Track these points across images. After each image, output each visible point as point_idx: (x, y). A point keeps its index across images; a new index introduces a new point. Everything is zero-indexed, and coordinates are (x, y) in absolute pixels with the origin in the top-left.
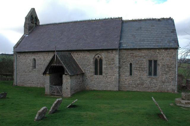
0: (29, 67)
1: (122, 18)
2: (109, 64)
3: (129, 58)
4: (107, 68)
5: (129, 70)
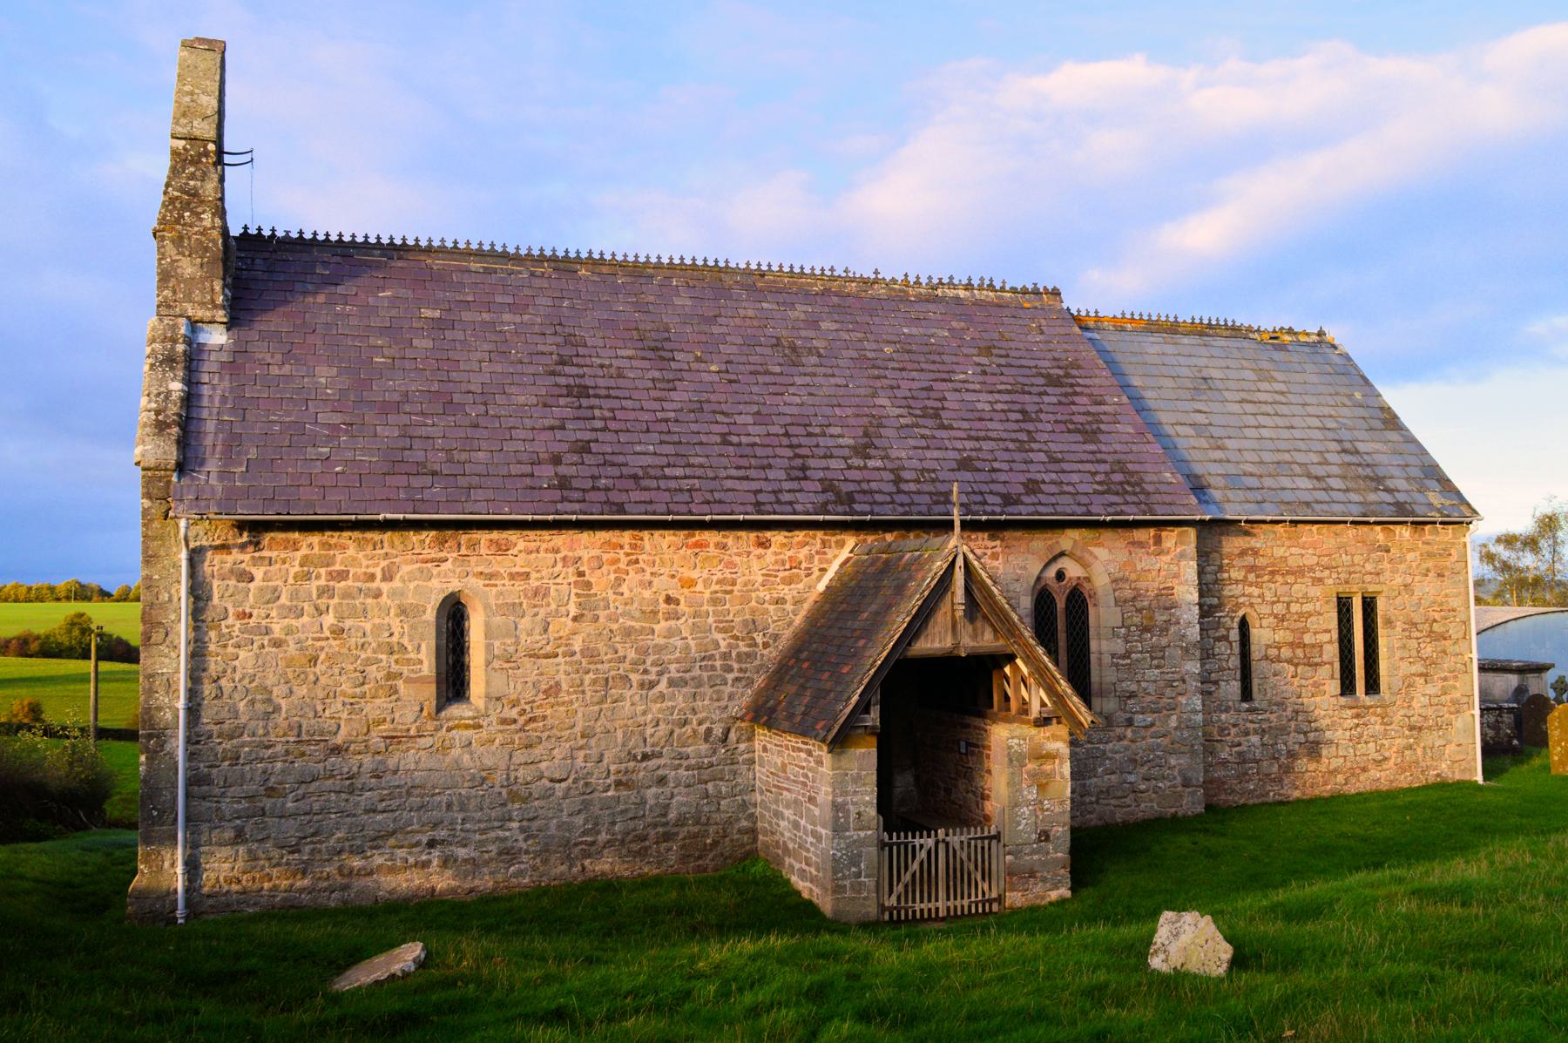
0: (394, 691)
1: (1056, 293)
2: (1146, 629)
3: (1237, 582)
4: (1127, 655)
5: (1235, 662)
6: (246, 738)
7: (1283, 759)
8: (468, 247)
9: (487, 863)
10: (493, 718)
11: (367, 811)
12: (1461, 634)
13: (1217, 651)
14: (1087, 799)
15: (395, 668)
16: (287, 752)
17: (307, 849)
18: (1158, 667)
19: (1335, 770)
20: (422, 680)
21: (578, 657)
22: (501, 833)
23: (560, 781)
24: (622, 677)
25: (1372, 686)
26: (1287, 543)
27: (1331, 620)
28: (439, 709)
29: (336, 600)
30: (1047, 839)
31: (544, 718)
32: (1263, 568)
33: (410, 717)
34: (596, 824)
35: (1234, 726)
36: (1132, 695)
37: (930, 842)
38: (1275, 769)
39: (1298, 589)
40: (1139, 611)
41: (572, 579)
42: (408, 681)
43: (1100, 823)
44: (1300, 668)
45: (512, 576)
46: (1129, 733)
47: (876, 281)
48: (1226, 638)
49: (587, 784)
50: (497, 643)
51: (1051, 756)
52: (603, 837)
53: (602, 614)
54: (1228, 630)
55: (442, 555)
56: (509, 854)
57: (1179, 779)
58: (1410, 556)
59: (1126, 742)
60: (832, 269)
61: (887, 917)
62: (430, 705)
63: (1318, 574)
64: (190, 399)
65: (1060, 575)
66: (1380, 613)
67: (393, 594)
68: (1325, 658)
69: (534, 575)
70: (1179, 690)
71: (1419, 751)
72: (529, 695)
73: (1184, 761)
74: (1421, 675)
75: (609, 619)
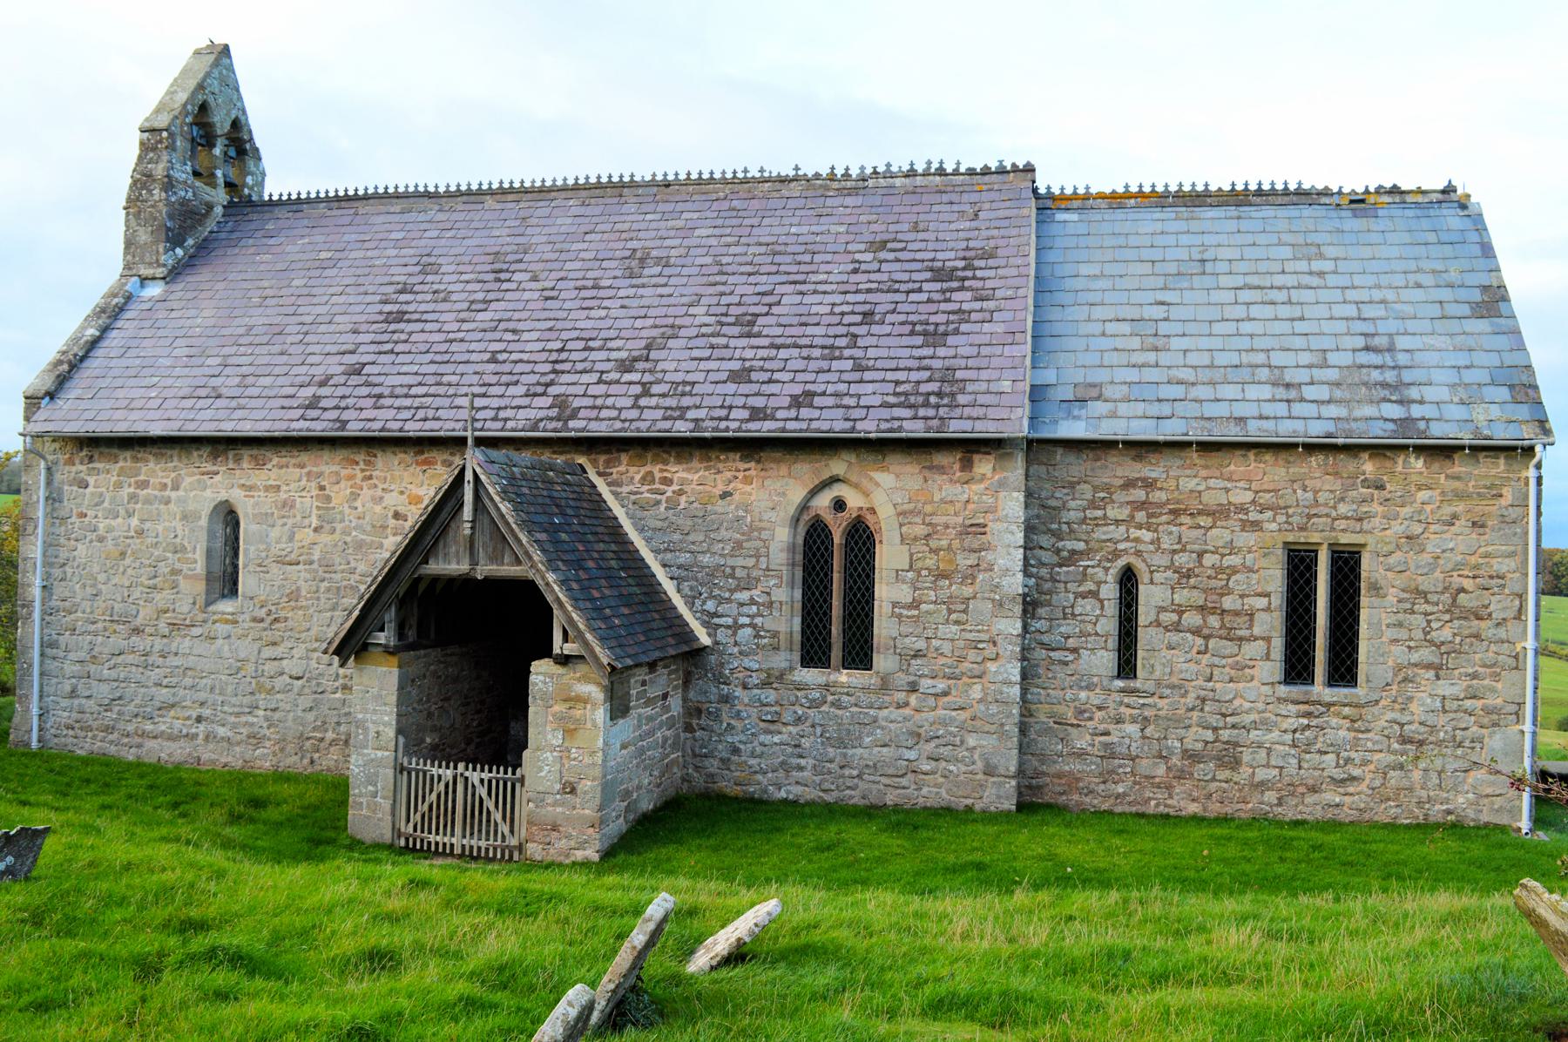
1: (1029, 169)
4: (915, 604)
5: (1109, 625)
6: (79, 614)
7: (1175, 760)
8: (1193, 190)
9: (238, 744)
10: (247, 617)
11: (157, 685)
12: (1510, 614)
13: (1078, 610)
14: (847, 772)
15: (178, 566)
16: (105, 629)
17: (116, 709)
18: (957, 622)
19: (1262, 783)
20: (195, 577)
21: (315, 566)
22: (251, 719)
23: (298, 678)
24: (352, 587)
25: (1344, 670)
26: (1204, 473)
27: (1275, 579)
28: (208, 604)
29: (139, 506)
30: (573, 791)
31: (286, 619)
32: (1162, 505)
33: (185, 609)
34: (324, 723)
35: (1100, 708)
36: (917, 654)
37: (450, 773)
38: (1161, 770)
39: (1219, 536)
40: (935, 551)
41: (315, 492)
42: (186, 577)
43: (862, 802)
44: (1212, 643)
45: (267, 489)
46: (913, 699)
47: (796, 179)
48: (1094, 594)
49: (318, 684)
50: (252, 549)
51: (583, 700)
52: (330, 735)
53: (339, 527)
54: (1099, 584)
55: (215, 468)
56: (256, 739)
57: (980, 765)
58: (1423, 495)
59: (907, 711)
60: (746, 171)
61: (403, 843)
62: (201, 600)
63: (1253, 516)
64: (94, 343)
65: (839, 505)
66: (1364, 575)
67: (180, 500)
68: (1257, 631)
69: (284, 488)
70: (987, 653)
71: (1417, 775)
72: (274, 598)
73: (989, 742)
74: (1428, 666)
75: (343, 533)
